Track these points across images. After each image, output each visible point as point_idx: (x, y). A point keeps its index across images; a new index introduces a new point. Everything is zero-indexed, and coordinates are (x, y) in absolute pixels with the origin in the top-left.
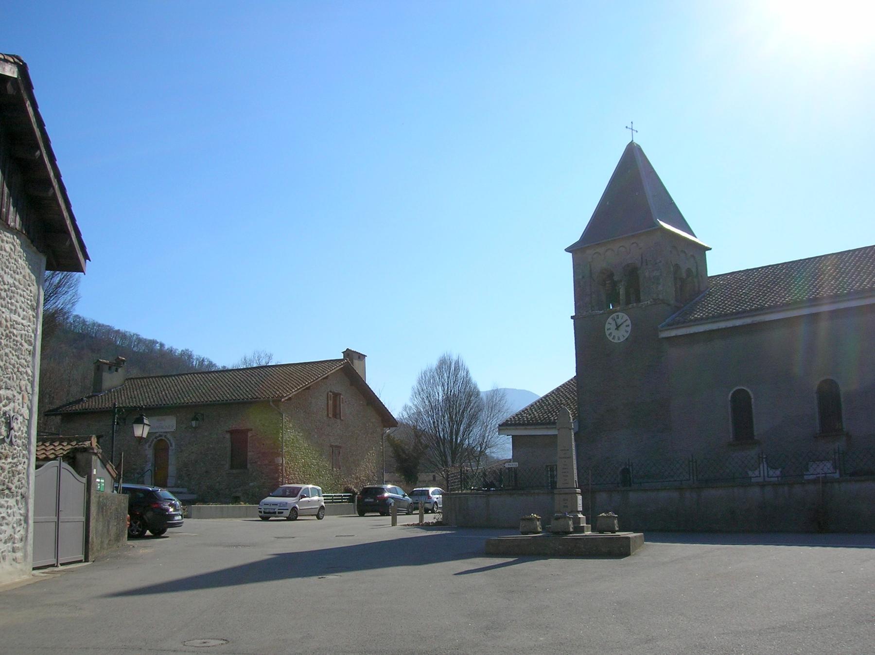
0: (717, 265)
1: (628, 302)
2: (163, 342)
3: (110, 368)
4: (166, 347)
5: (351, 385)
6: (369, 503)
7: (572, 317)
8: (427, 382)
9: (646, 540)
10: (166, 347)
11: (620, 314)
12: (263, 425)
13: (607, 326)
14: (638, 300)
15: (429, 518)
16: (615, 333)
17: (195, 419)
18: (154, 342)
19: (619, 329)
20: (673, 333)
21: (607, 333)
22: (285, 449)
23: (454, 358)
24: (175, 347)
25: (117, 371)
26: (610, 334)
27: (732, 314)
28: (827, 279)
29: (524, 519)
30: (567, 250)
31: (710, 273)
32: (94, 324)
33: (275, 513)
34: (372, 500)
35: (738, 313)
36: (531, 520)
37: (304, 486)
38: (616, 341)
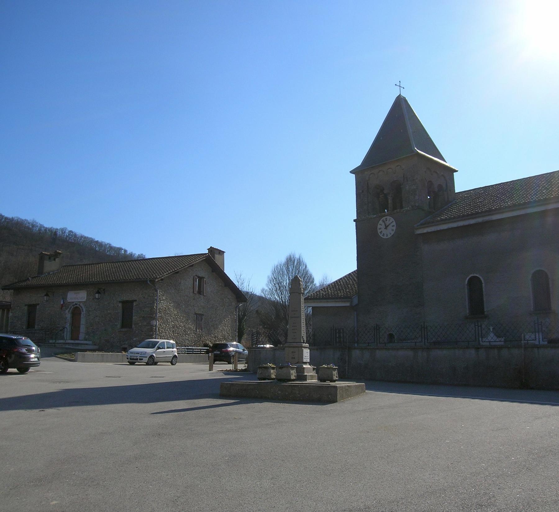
0: (462, 184)
1: (395, 208)
2: (126, 249)
3: (50, 258)
4: (128, 252)
5: (212, 272)
6: (219, 354)
7: (354, 221)
8: (278, 272)
9: (367, 389)
10: (128, 252)
11: (388, 217)
12: (144, 298)
13: (379, 226)
14: (402, 207)
15: (241, 366)
16: (385, 232)
17: (98, 292)
18: (120, 249)
19: (387, 228)
20: (425, 231)
21: (379, 231)
22: (159, 315)
23: (297, 256)
24: (134, 252)
25: (54, 260)
26: (381, 232)
27: (468, 215)
28: (541, 190)
29: (260, 368)
30: (351, 172)
31: (457, 191)
32: (82, 237)
33: (137, 359)
34: (219, 353)
35: (472, 214)
36: (267, 368)
37: (161, 341)
38: (385, 237)
